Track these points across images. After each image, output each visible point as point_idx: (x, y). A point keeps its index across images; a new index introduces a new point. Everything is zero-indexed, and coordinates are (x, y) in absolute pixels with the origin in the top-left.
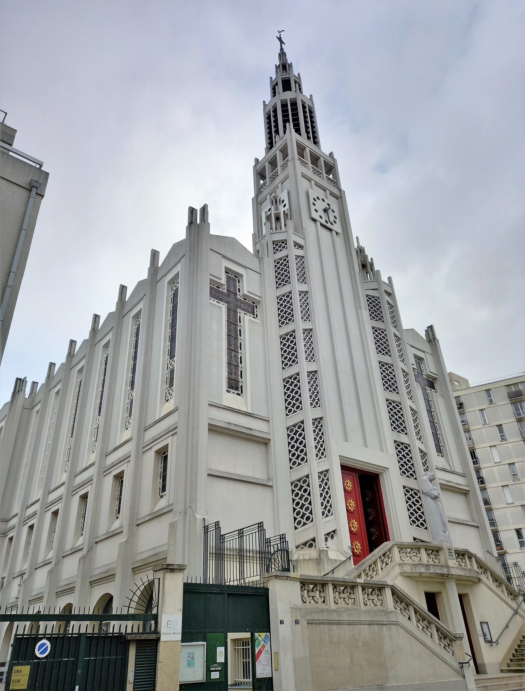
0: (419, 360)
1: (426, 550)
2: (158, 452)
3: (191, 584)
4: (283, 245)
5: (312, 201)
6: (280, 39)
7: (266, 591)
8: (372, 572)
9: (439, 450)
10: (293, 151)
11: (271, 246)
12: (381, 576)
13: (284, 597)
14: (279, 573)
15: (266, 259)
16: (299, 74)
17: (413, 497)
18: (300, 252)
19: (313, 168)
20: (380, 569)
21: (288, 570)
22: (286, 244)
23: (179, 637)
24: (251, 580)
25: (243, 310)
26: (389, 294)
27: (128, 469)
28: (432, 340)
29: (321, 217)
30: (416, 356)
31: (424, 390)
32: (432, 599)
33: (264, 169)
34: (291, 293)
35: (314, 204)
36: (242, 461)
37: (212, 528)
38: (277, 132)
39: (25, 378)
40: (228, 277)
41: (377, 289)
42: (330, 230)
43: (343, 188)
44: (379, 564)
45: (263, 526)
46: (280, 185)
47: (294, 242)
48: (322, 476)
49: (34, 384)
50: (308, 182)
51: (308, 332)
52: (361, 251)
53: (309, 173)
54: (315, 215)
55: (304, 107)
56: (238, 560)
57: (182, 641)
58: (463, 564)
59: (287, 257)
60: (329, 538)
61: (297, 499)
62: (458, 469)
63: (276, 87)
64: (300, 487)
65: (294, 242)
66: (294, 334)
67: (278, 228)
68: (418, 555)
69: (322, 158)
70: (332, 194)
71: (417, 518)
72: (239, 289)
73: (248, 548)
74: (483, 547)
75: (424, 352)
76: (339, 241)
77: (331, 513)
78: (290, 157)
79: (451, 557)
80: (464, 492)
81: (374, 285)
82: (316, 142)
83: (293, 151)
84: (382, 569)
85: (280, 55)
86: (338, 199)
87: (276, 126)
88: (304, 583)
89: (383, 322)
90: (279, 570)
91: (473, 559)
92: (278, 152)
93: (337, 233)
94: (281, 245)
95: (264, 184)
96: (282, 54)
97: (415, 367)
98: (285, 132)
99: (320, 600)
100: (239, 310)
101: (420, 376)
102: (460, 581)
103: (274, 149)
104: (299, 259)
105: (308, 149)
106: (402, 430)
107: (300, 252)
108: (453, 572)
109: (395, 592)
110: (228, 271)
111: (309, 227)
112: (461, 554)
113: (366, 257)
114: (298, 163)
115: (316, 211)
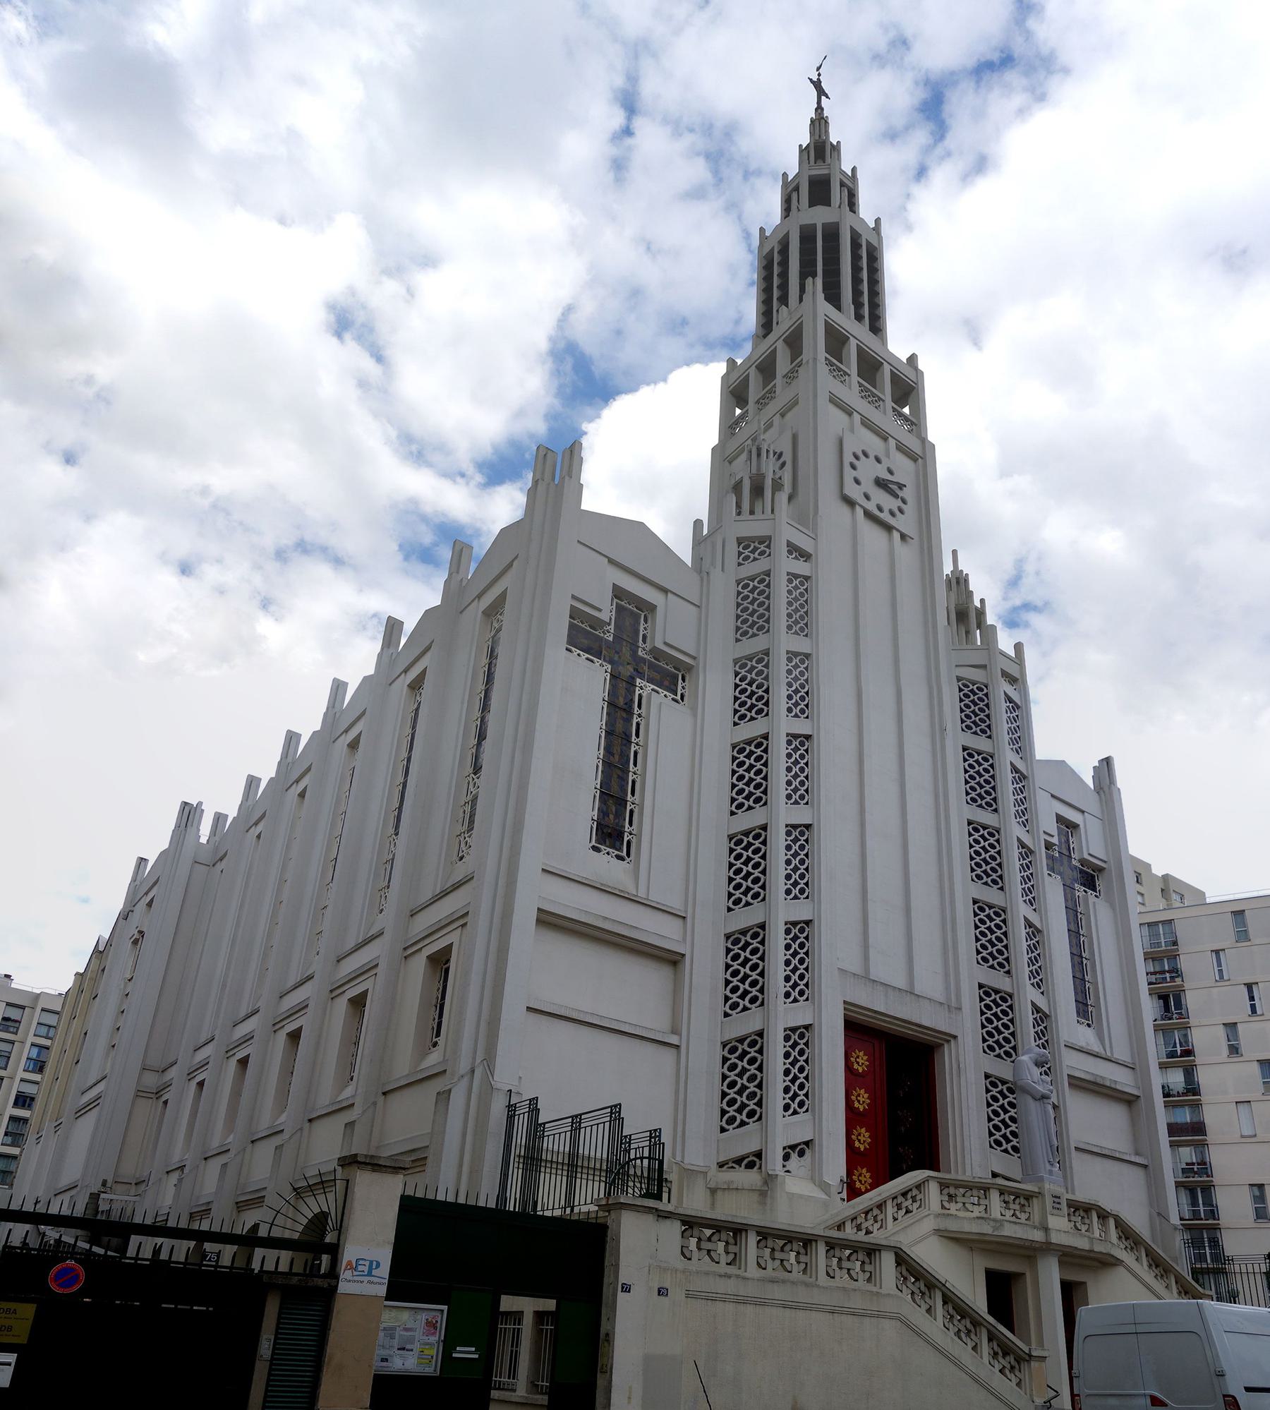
0: (1068, 826)
1: (1001, 1194)
2: (433, 959)
3: (409, 1196)
4: (762, 547)
5: (848, 458)
6: (817, 85)
7: (604, 1228)
8: (871, 1222)
9: (1085, 1009)
10: (815, 344)
11: (732, 548)
12: (890, 1232)
13: (641, 1246)
14: (640, 1202)
15: (716, 574)
16: (854, 170)
17: (1002, 1093)
18: (801, 567)
19: (860, 385)
20: (890, 1219)
21: (658, 1197)
22: (769, 547)
23: (382, 1291)
24: (584, 1209)
25: (650, 681)
26: (1012, 680)
27: (375, 987)
28: (1106, 789)
29: (867, 497)
30: (1060, 819)
31: (1068, 888)
32: (1002, 1290)
33: (745, 382)
34: (767, 654)
35: (853, 467)
36: (630, 992)
37: (523, 1110)
38: (784, 300)
39: (200, 804)
40: (620, 609)
41: (984, 667)
42: (888, 528)
43: (932, 436)
44: (890, 1209)
45: (659, 1136)
46: (777, 419)
47: (789, 544)
48: (795, 1037)
49: (219, 818)
50: (844, 417)
51: (801, 741)
52: (959, 582)
53: (851, 393)
54: (853, 491)
55: (856, 245)
56: (565, 1173)
57: (387, 1299)
58: (1084, 1228)
59: (769, 575)
60: (794, 1156)
61: (732, 1076)
62: (1122, 1053)
63: (794, 196)
64: (743, 1056)
65: (789, 544)
66: (765, 743)
67: (758, 509)
68: (983, 1202)
69: (886, 366)
70: (901, 448)
71: (1005, 1133)
72: (645, 637)
73: (586, 1153)
74: (1151, 1205)
75: (1083, 812)
76: (906, 555)
77: (805, 1109)
78: (806, 355)
79: (1055, 1211)
80: (1126, 1097)
81: (978, 658)
82: (877, 326)
83: (815, 344)
84: (895, 1219)
85: (812, 121)
86: (915, 460)
87: (784, 287)
88: (690, 1224)
89: (990, 737)
90: (641, 1196)
91: (1112, 1222)
92: (780, 345)
93: (903, 537)
94: (755, 549)
95: (742, 417)
96: (819, 123)
97: (1055, 840)
98: (801, 300)
99: (724, 1259)
100: (638, 680)
101: (1065, 859)
102: (1068, 1257)
103: (772, 337)
104: (796, 582)
105: (853, 342)
106: (1001, 965)
107: (801, 567)
108: (1055, 1238)
109: (902, 1260)
110: (618, 593)
111: (833, 515)
112: (1081, 1209)
113: (970, 594)
114: (823, 369)
115: (857, 482)
